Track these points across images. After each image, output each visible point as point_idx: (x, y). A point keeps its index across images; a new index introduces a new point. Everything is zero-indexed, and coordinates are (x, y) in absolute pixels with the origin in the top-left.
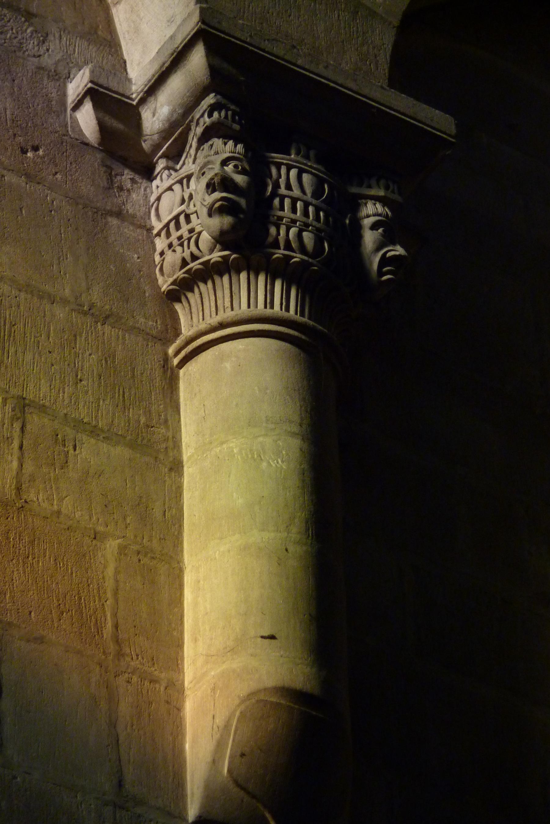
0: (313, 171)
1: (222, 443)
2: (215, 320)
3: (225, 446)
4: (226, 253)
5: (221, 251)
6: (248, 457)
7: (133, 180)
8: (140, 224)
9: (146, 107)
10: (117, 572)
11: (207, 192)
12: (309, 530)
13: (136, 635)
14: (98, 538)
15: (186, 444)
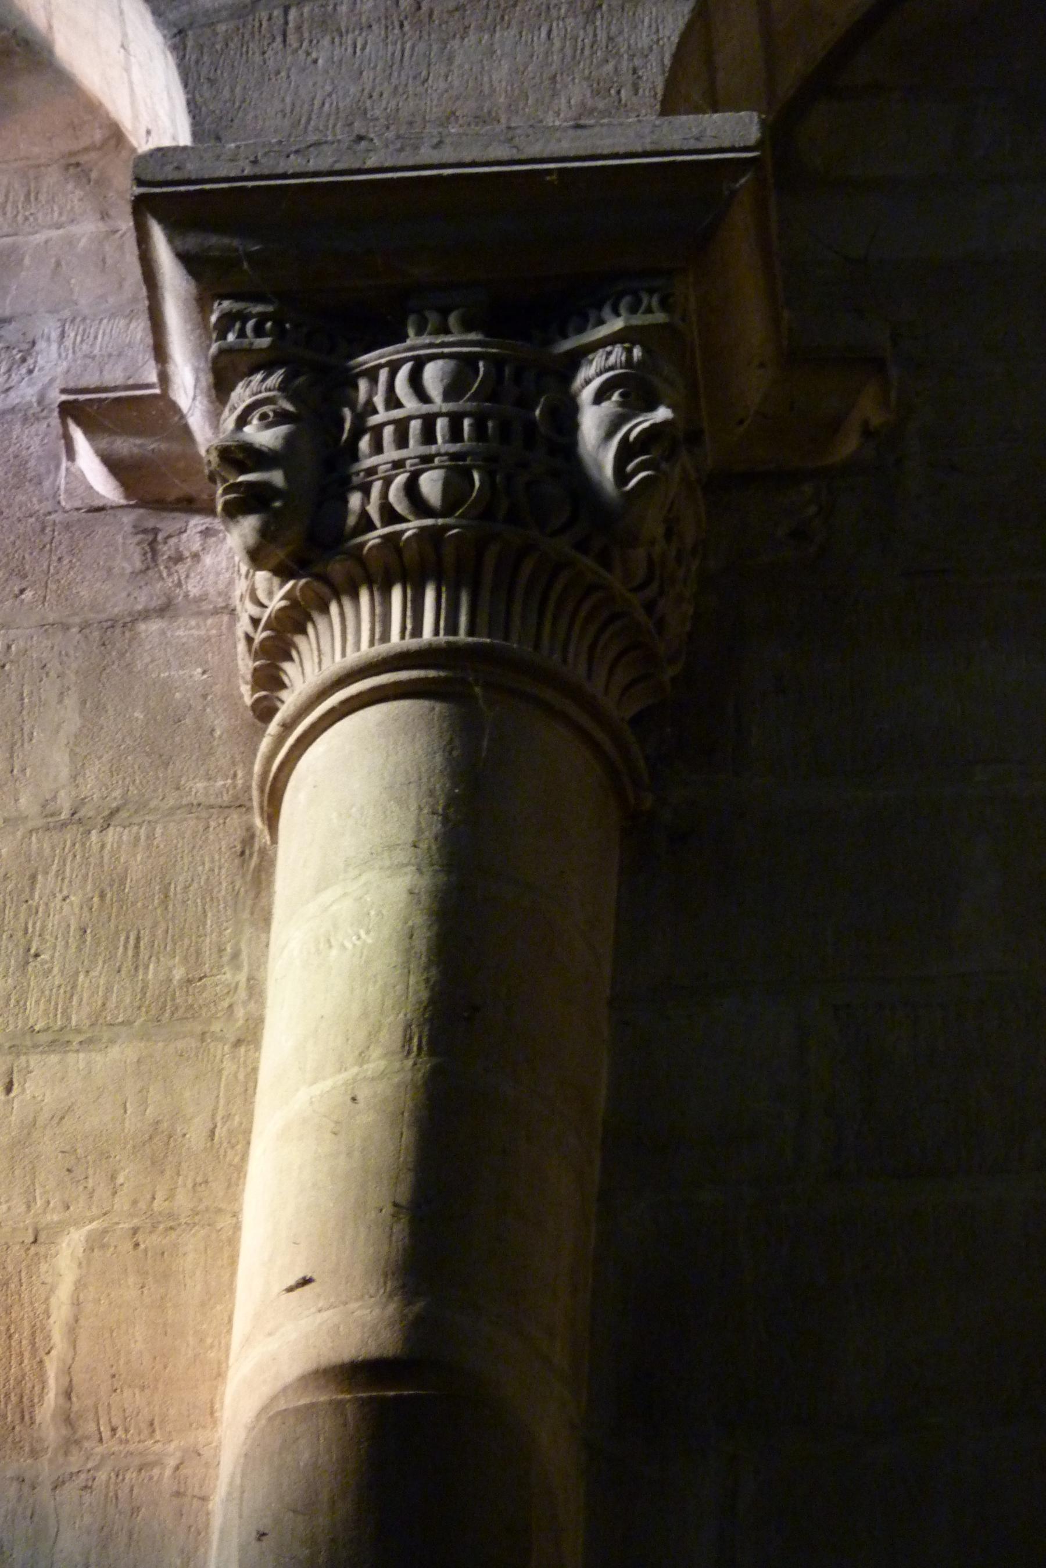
0: (446, 350)
4: (290, 584)
5: (281, 586)
8: (215, 607)
10: (80, 1285)
12: (411, 1039)
13: (115, 1391)
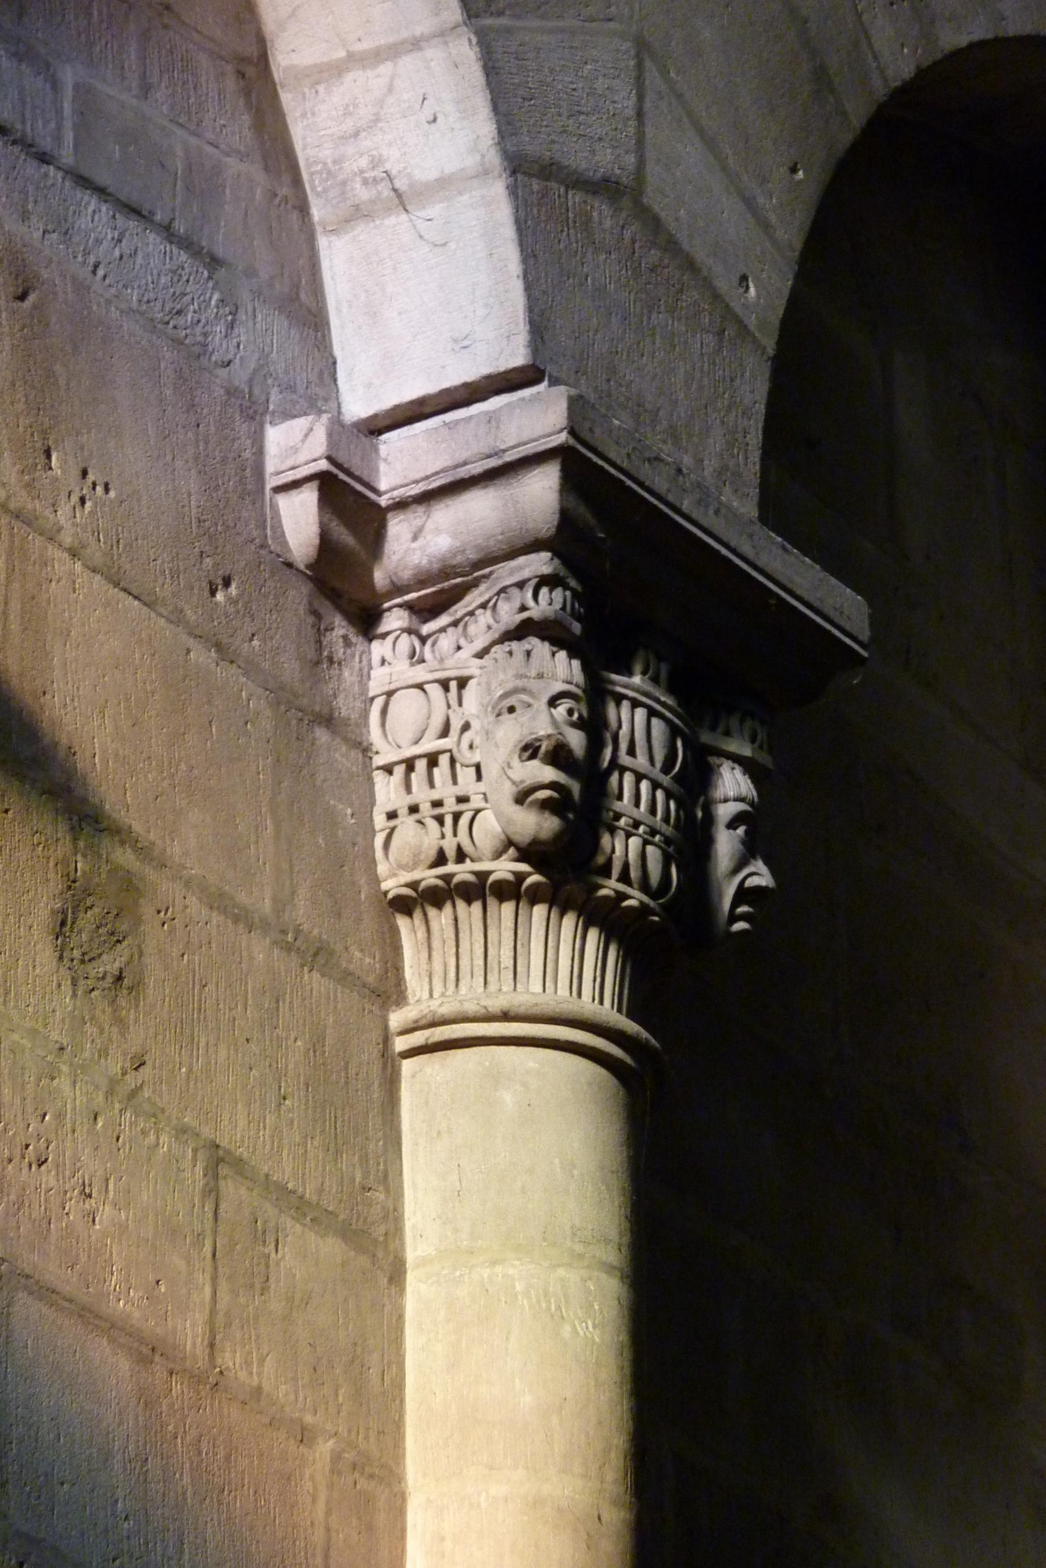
1: (494, 1263)
2: (496, 1004)
3: (499, 1269)
5: (518, 860)
6: (540, 1306)
7: (347, 642)
9: (402, 517)
11: (520, 756)
14: (305, 1441)
15: (414, 1227)
